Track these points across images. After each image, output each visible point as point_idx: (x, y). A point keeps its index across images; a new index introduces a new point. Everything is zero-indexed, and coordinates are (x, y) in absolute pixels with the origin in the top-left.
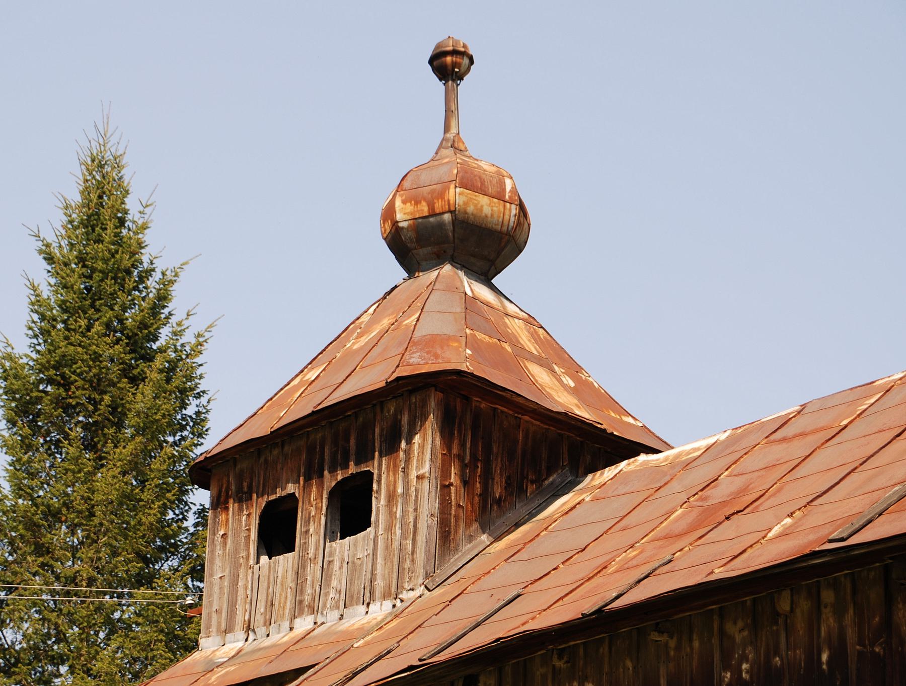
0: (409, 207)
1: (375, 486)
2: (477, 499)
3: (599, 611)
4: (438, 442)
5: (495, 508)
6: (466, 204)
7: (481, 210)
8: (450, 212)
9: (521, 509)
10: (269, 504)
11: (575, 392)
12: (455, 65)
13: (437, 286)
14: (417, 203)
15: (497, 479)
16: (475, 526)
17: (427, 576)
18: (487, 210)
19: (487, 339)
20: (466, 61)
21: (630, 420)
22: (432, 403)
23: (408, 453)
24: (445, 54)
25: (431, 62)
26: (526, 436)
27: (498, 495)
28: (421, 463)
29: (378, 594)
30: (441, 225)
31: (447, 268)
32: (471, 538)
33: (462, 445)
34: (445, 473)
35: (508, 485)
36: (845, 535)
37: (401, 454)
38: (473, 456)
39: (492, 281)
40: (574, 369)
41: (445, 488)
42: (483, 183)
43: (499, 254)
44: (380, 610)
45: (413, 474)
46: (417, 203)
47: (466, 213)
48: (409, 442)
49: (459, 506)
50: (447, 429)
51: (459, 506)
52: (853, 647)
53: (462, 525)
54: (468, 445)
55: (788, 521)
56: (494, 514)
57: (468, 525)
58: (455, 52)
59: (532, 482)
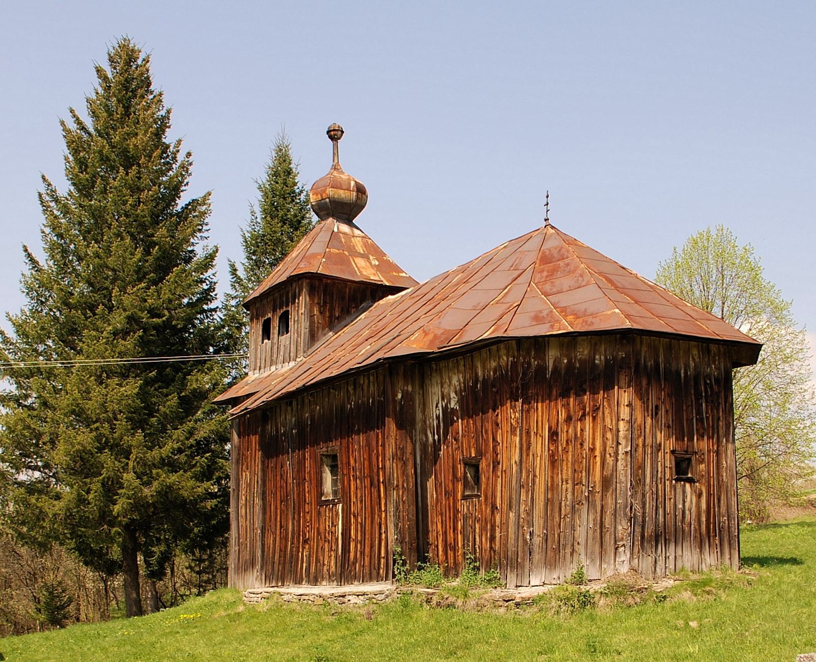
0: (315, 197)
1: (290, 317)
2: (327, 319)
3: (304, 385)
4: (308, 299)
5: (336, 321)
6: (334, 194)
7: (341, 196)
8: (329, 198)
9: (348, 319)
10: (265, 320)
11: (378, 268)
12: (335, 135)
13: (323, 229)
14: (317, 195)
15: (336, 309)
16: (327, 329)
17: (304, 352)
18: (343, 196)
19: (337, 251)
20: (340, 133)
21: (404, 275)
22: (304, 285)
23: (298, 303)
24: (331, 131)
25: (328, 132)
26: (350, 289)
27: (337, 315)
28: (302, 309)
29: (292, 359)
30: (326, 203)
31: (331, 219)
32: (325, 335)
33: (320, 298)
34: (311, 310)
35: (342, 310)
36: (360, 361)
37: (296, 304)
38: (325, 302)
39: (353, 221)
40: (379, 254)
41: (312, 316)
42: (341, 184)
43: (351, 211)
44: (292, 364)
45: (300, 312)
46: (317, 195)
47: (334, 198)
48: (299, 300)
49: (318, 322)
50: (311, 293)
51: (318, 322)
52: (377, 398)
53: (320, 330)
54: (322, 298)
55: (369, 347)
56: (335, 323)
57: (323, 329)
58: (334, 130)
59: (354, 308)
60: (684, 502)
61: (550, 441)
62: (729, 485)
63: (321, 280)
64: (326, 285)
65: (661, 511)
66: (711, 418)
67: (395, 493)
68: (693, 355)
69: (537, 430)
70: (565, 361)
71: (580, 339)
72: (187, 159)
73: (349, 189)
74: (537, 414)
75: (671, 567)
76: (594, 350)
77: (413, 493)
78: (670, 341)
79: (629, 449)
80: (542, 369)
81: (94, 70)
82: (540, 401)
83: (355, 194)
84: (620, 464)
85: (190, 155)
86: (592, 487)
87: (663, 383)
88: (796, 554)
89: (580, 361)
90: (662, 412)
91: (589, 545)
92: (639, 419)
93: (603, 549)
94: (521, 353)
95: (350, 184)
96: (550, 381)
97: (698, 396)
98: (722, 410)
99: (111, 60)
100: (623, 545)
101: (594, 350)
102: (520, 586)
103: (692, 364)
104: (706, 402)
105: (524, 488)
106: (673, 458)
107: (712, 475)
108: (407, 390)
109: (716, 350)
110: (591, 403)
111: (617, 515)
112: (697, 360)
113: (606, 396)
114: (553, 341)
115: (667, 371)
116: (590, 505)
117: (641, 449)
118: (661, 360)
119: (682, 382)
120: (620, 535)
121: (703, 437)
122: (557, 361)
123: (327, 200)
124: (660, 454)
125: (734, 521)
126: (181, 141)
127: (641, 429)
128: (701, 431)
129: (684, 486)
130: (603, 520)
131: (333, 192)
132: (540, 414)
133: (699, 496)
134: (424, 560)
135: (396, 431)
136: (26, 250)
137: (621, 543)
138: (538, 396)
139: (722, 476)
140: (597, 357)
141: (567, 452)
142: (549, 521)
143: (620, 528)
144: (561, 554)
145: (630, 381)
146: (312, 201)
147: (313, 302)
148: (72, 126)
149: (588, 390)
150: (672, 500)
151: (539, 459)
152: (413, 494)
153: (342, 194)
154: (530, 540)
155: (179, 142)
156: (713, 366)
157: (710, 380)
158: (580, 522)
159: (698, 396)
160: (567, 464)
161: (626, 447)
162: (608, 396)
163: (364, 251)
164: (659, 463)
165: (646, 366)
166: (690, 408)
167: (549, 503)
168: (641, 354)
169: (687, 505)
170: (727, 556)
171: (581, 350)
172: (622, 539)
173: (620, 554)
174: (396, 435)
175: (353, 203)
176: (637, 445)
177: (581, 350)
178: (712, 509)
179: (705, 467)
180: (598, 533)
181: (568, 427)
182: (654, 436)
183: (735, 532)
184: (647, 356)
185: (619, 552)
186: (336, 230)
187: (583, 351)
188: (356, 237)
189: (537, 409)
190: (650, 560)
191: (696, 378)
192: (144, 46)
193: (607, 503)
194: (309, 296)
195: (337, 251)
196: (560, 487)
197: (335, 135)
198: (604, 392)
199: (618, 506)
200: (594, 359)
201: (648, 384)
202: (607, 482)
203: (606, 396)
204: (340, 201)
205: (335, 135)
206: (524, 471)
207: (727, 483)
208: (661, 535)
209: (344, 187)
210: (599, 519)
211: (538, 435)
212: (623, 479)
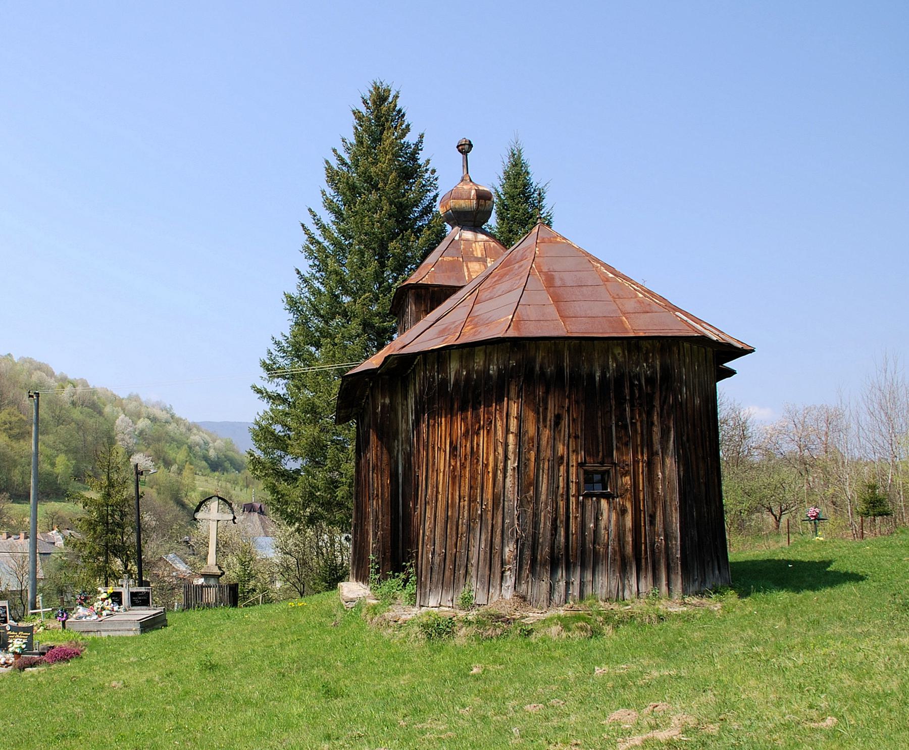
18: (464, 205)
19: (451, 259)
25: (458, 147)
30: (450, 214)
42: (461, 195)
60: (597, 520)
61: (451, 456)
62: (668, 499)
63: (428, 289)
64: (433, 292)
65: (562, 532)
66: (639, 424)
67: (375, 503)
68: (613, 353)
69: (441, 445)
70: (465, 373)
71: (477, 349)
72: (431, 176)
73: (469, 199)
74: (441, 428)
75: (575, 594)
76: (488, 361)
77: (388, 503)
78: (580, 343)
79: (516, 464)
80: (444, 382)
81: (352, 113)
82: (443, 416)
83: (475, 202)
84: (509, 481)
85: (435, 172)
86: (485, 505)
87: (567, 389)
88: (860, 571)
89: (477, 372)
90: (565, 421)
91: (480, 566)
92: (531, 430)
93: (492, 572)
94: (428, 367)
95: (470, 193)
96: (452, 393)
97: (620, 402)
98: (657, 414)
99: (365, 102)
100: (509, 569)
101: (488, 361)
102: (423, 606)
103: (612, 365)
104: (632, 406)
105: (429, 505)
106: (581, 472)
107: (641, 489)
108: (384, 403)
109: (649, 347)
110: (486, 416)
111: (505, 536)
112: (621, 359)
113: (498, 408)
114: (455, 354)
115: (575, 379)
116: (483, 524)
117: (533, 464)
118: (565, 365)
119: (597, 385)
120: (506, 557)
121: (626, 444)
122: (458, 373)
123: (450, 211)
124: (562, 468)
125: (676, 541)
126: (429, 160)
127: (533, 442)
128: (625, 440)
129: (598, 502)
130: (493, 540)
131: (454, 203)
132: (443, 428)
133: (623, 511)
134: (398, 568)
135: (377, 442)
136: (299, 273)
137: (508, 567)
138: (442, 410)
139: (658, 489)
140: (491, 367)
141: (465, 467)
142: (448, 539)
143: (507, 550)
144: (456, 575)
145: (520, 391)
146: (441, 213)
147: (420, 310)
148: (335, 163)
149: (482, 403)
150: (579, 519)
151: (442, 474)
152: (388, 505)
153: (463, 204)
154: (432, 558)
155: (428, 162)
156: (645, 365)
157: (639, 381)
158: (474, 541)
159: (620, 402)
160: (465, 481)
161: (514, 463)
162: (500, 408)
163: (482, 255)
164: (561, 479)
165: (543, 373)
166: (609, 414)
167: (449, 521)
168: (535, 362)
169: (603, 524)
170: (664, 582)
171: (478, 361)
172: (509, 563)
173: (506, 578)
174: (377, 446)
175: (474, 211)
176: (529, 460)
177: (478, 361)
178: (643, 528)
179: (631, 479)
180: (488, 554)
181: (466, 441)
182: (554, 448)
183: (676, 554)
184: (546, 361)
185: (506, 576)
186: (457, 238)
187: (479, 362)
188: (478, 242)
189: (441, 423)
190: (544, 586)
191: (619, 380)
192: (393, 83)
193: (497, 522)
194: (415, 305)
195: (451, 259)
196: (457, 504)
197: (465, 148)
198: (496, 405)
199: (506, 525)
200: (489, 370)
201: (547, 392)
202: (497, 500)
203: (498, 408)
204: (461, 210)
205: (465, 148)
206: (430, 488)
207: (664, 496)
208: (562, 557)
209: (464, 198)
210: (489, 538)
211: (442, 450)
212: (511, 497)
